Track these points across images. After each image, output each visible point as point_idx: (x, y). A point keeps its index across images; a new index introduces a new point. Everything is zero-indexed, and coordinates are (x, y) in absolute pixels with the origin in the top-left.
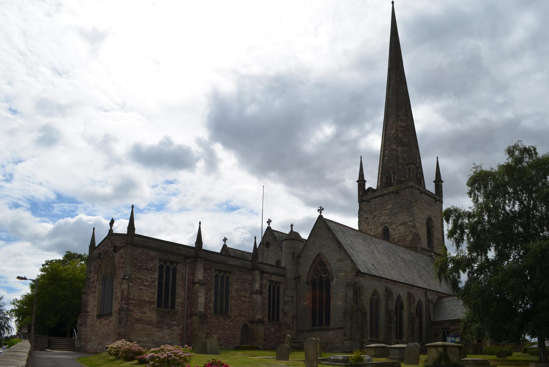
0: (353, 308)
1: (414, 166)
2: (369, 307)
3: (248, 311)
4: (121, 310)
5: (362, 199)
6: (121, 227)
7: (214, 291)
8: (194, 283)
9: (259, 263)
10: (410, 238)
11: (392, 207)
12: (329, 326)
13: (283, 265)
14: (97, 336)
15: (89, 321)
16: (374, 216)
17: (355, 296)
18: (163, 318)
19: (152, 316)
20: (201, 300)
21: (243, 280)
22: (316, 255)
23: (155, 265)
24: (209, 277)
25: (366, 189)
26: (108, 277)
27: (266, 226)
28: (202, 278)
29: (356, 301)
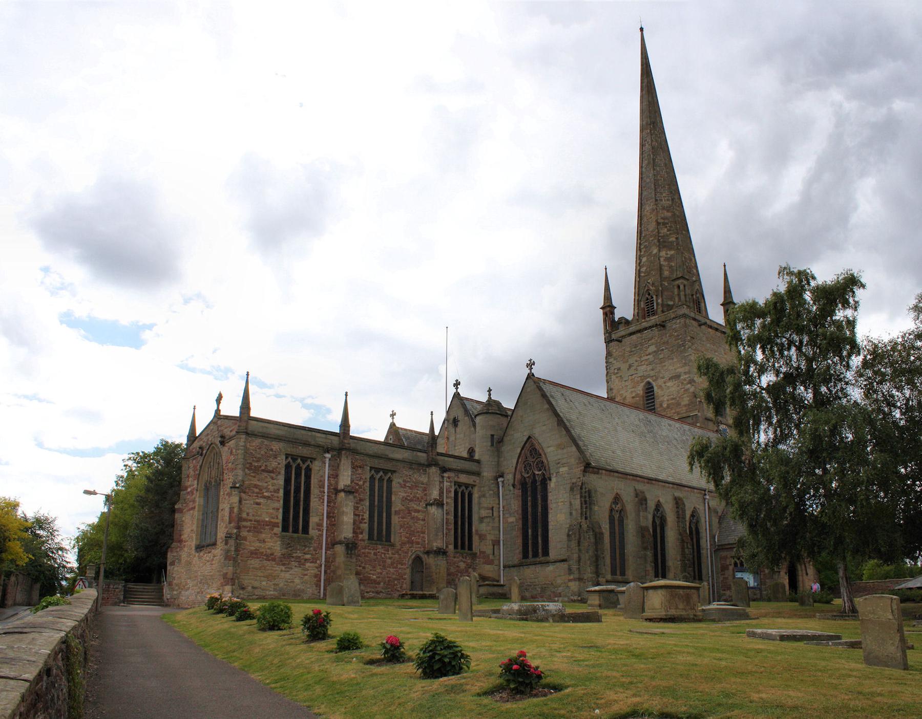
0: (581, 526)
1: (685, 282)
2: (608, 524)
3: (422, 535)
4: (228, 537)
5: (611, 337)
6: (231, 409)
7: (368, 504)
8: (337, 491)
9: (438, 455)
10: (686, 401)
11: (655, 349)
12: (548, 558)
13: (476, 457)
14: (195, 580)
15: (184, 555)
16: (630, 366)
17: (584, 506)
18: (290, 549)
19: (274, 543)
20: (348, 518)
21: (413, 484)
22: (525, 439)
23: (279, 464)
24: (360, 480)
25: (616, 319)
26: (213, 483)
27: (452, 391)
28: (349, 483)
29: (586, 514)
